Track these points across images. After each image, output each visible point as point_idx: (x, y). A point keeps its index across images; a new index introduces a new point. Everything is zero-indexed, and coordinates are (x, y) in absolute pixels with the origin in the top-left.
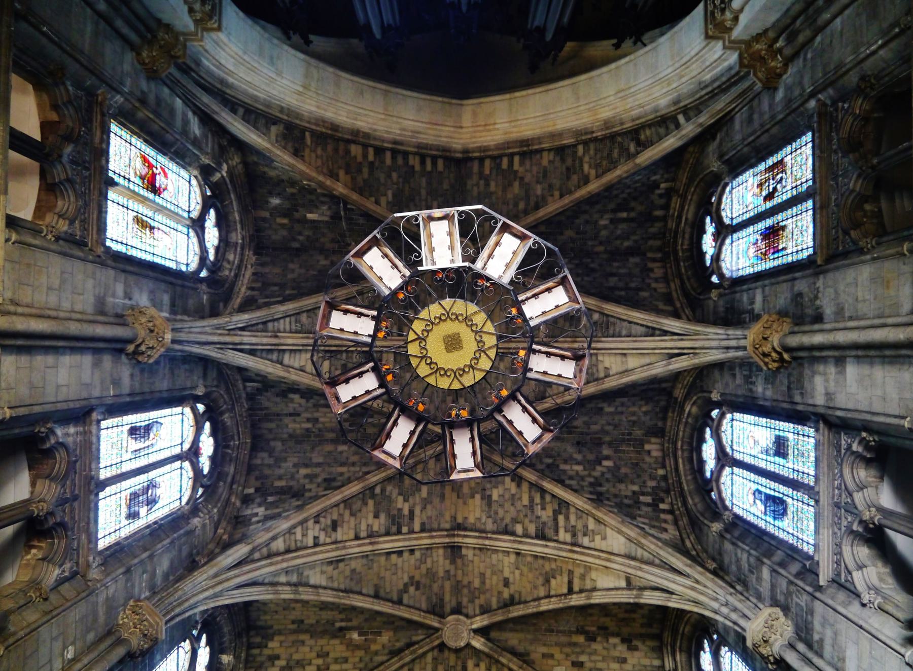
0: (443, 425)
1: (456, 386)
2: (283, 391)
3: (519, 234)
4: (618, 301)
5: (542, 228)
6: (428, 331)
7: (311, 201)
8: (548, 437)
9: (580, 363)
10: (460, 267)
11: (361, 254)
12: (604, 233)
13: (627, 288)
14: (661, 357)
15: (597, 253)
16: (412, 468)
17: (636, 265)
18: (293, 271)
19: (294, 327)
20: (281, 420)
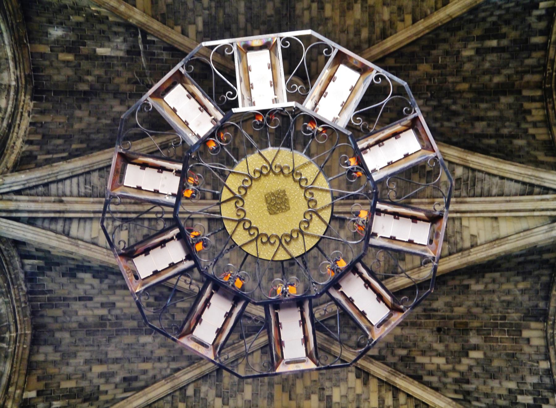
0: (266, 305)
1: (282, 256)
2: (71, 269)
3: (358, 66)
4: (486, 151)
5: (391, 62)
6: (246, 189)
7: (102, 32)
8: (397, 318)
9: (436, 226)
10: (284, 108)
11: (161, 94)
12: (468, 66)
13: (498, 135)
14: (542, 221)
15: (461, 92)
16: (232, 362)
17: (510, 106)
18: (81, 119)
19: (82, 190)
20: (68, 305)
